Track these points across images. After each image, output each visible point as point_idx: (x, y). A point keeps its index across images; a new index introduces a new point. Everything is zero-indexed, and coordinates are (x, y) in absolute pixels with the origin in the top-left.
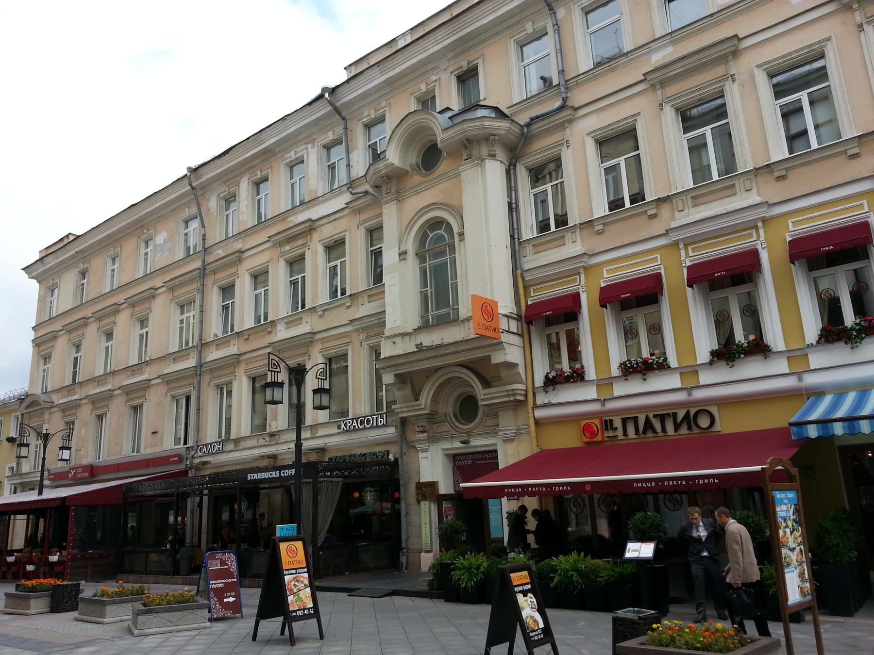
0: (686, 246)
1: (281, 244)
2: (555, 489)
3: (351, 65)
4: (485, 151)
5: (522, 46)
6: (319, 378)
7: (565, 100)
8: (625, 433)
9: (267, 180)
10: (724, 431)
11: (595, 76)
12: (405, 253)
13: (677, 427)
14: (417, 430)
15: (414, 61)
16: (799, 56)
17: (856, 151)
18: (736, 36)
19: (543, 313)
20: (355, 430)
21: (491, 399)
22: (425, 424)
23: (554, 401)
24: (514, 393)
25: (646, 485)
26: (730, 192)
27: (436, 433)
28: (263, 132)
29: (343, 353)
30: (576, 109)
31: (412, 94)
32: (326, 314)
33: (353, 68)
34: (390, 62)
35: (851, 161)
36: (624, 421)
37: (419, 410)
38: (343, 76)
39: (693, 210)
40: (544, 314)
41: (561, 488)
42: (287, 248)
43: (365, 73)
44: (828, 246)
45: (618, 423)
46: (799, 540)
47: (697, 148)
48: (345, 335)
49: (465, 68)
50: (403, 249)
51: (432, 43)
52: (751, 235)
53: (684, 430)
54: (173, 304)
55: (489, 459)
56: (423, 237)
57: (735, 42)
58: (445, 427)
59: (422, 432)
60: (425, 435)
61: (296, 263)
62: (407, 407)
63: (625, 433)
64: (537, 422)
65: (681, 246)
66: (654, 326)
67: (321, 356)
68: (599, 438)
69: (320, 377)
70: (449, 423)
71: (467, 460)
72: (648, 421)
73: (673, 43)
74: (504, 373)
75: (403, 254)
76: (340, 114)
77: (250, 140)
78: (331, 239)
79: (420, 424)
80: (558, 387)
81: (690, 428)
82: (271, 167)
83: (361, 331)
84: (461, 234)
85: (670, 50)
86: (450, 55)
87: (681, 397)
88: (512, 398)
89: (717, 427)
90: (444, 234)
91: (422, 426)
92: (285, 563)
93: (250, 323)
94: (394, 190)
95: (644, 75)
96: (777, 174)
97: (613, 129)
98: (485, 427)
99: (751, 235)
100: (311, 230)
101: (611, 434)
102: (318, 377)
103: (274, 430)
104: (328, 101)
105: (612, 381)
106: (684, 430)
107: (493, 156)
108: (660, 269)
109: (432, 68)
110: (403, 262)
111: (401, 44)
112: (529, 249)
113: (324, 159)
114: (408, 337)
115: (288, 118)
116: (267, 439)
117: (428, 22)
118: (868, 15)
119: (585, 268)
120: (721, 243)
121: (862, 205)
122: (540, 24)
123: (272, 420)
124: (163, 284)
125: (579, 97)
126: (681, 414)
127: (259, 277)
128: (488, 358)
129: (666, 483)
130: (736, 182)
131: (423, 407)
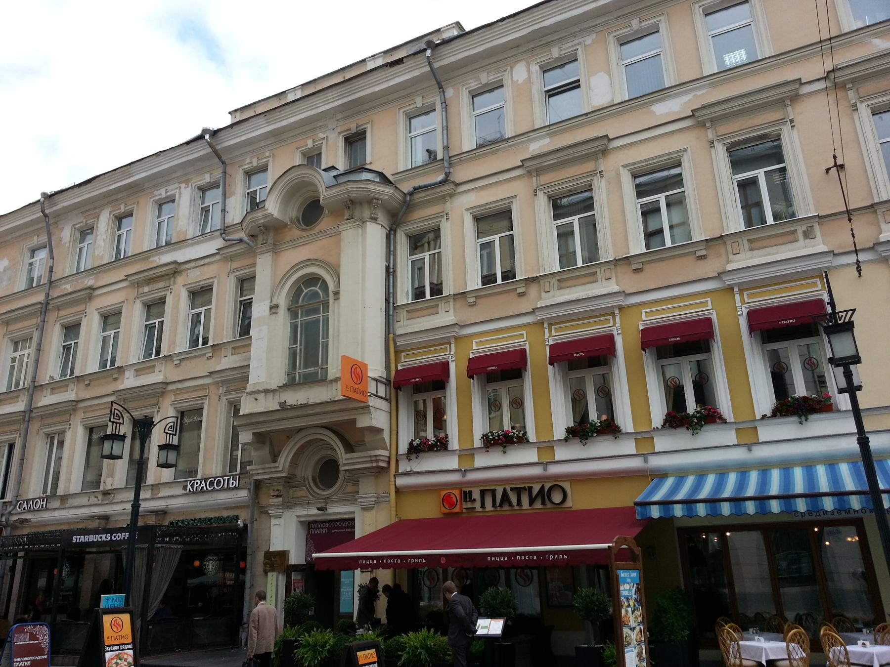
0: (550, 325)
1: (139, 284)
2: (410, 561)
3: (236, 111)
4: (367, 213)
5: (410, 118)
6: (167, 433)
7: (447, 175)
8: (483, 505)
9: (131, 215)
10: (574, 509)
11: (478, 156)
12: (277, 306)
13: (531, 503)
14: (272, 494)
15: (303, 116)
16: (660, 161)
17: (703, 253)
18: (607, 136)
19: (781, 321)
20: (202, 491)
21: (353, 464)
22: (281, 488)
23: (416, 470)
24: (377, 459)
25: (500, 559)
26: (791, 238)
27: (293, 498)
28: (132, 165)
29: (198, 406)
30: (457, 185)
31: (297, 148)
32: (183, 363)
33: (238, 114)
34: (278, 114)
35: (699, 261)
36: (483, 493)
37: (277, 472)
38: (227, 121)
39: (558, 292)
40: (413, 380)
41: (556, 557)
42: (146, 289)
43: (251, 120)
44: (676, 337)
45: (476, 495)
46: (640, 619)
47: (565, 235)
48: (203, 387)
49: (354, 131)
50: (275, 302)
51: (323, 102)
52: (815, 284)
53: (538, 505)
54: (232, 276)
55: (346, 528)
56: (296, 292)
57: (605, 141)
58: (302, 492)
59: (278, 496)
60: (280, 499)
61: (155, 307)
62: (263, 469)
63: (483, 505)
64: (398, 491)
65: (546, 325)
66: (810, 360)
67: (173, 409)
68: (457, 509)
69: (169, 432)
70: (307, 488)
71: (323, 528)
72: (505, 493)
73: (551, 135)
74: (368, 438)
75: (274, 308)
76: (219, 157)
77: (117, 171)
78: (198, 284)
79: (276, 488)
80: (421, 455)
81: (543, 503)
82: (138, 202)
83: (220, 385)
84: (337, 293)
85: (547, 141)
86: (339, 116)
87: (537, 471)
88: (374, 464)
89: (569, 503)
90: (319, 291)
91: (278, 490)
92: (108, 638)
93: (93, 367)
94: (270, 241)
95: (692, 111)
96: (634, 267)
97: (490, 208)
98: (344, 494)
99: (815, 284)
100: (175, 272)
101: (469, 505)
102: (167, 431)
103: (109, 487)
104: (208, 143)
105: (474, 452)
106: (538, 505)
107: (374, 219)
108: (525, 345)
109: (320, 126)
110: (273, 316)
111: (291, 98)
112: (403, 314)
113: (198, 201)
114: (271, 394)
115: (162, 154)
116: (100, 497)
117: (321, 81)
118: (719, 134)
119: (456, 338)
120: (596, 323)
121: (706, 302)
122: (429, 100)
123: (108, 477)
124: (125, 278)
125: (461, 174)
126: (536, 488)
127: (110, 318)
128: (354, 421)
129: (518, 558)
130: (598, 271)
131: (280, 469)
